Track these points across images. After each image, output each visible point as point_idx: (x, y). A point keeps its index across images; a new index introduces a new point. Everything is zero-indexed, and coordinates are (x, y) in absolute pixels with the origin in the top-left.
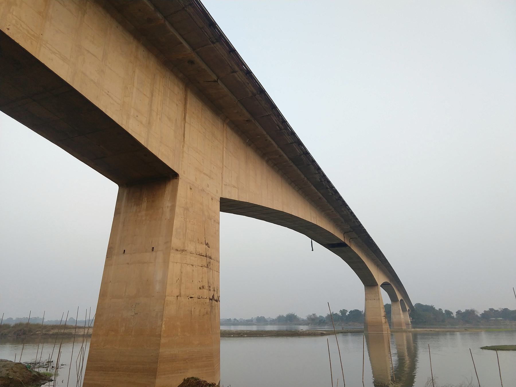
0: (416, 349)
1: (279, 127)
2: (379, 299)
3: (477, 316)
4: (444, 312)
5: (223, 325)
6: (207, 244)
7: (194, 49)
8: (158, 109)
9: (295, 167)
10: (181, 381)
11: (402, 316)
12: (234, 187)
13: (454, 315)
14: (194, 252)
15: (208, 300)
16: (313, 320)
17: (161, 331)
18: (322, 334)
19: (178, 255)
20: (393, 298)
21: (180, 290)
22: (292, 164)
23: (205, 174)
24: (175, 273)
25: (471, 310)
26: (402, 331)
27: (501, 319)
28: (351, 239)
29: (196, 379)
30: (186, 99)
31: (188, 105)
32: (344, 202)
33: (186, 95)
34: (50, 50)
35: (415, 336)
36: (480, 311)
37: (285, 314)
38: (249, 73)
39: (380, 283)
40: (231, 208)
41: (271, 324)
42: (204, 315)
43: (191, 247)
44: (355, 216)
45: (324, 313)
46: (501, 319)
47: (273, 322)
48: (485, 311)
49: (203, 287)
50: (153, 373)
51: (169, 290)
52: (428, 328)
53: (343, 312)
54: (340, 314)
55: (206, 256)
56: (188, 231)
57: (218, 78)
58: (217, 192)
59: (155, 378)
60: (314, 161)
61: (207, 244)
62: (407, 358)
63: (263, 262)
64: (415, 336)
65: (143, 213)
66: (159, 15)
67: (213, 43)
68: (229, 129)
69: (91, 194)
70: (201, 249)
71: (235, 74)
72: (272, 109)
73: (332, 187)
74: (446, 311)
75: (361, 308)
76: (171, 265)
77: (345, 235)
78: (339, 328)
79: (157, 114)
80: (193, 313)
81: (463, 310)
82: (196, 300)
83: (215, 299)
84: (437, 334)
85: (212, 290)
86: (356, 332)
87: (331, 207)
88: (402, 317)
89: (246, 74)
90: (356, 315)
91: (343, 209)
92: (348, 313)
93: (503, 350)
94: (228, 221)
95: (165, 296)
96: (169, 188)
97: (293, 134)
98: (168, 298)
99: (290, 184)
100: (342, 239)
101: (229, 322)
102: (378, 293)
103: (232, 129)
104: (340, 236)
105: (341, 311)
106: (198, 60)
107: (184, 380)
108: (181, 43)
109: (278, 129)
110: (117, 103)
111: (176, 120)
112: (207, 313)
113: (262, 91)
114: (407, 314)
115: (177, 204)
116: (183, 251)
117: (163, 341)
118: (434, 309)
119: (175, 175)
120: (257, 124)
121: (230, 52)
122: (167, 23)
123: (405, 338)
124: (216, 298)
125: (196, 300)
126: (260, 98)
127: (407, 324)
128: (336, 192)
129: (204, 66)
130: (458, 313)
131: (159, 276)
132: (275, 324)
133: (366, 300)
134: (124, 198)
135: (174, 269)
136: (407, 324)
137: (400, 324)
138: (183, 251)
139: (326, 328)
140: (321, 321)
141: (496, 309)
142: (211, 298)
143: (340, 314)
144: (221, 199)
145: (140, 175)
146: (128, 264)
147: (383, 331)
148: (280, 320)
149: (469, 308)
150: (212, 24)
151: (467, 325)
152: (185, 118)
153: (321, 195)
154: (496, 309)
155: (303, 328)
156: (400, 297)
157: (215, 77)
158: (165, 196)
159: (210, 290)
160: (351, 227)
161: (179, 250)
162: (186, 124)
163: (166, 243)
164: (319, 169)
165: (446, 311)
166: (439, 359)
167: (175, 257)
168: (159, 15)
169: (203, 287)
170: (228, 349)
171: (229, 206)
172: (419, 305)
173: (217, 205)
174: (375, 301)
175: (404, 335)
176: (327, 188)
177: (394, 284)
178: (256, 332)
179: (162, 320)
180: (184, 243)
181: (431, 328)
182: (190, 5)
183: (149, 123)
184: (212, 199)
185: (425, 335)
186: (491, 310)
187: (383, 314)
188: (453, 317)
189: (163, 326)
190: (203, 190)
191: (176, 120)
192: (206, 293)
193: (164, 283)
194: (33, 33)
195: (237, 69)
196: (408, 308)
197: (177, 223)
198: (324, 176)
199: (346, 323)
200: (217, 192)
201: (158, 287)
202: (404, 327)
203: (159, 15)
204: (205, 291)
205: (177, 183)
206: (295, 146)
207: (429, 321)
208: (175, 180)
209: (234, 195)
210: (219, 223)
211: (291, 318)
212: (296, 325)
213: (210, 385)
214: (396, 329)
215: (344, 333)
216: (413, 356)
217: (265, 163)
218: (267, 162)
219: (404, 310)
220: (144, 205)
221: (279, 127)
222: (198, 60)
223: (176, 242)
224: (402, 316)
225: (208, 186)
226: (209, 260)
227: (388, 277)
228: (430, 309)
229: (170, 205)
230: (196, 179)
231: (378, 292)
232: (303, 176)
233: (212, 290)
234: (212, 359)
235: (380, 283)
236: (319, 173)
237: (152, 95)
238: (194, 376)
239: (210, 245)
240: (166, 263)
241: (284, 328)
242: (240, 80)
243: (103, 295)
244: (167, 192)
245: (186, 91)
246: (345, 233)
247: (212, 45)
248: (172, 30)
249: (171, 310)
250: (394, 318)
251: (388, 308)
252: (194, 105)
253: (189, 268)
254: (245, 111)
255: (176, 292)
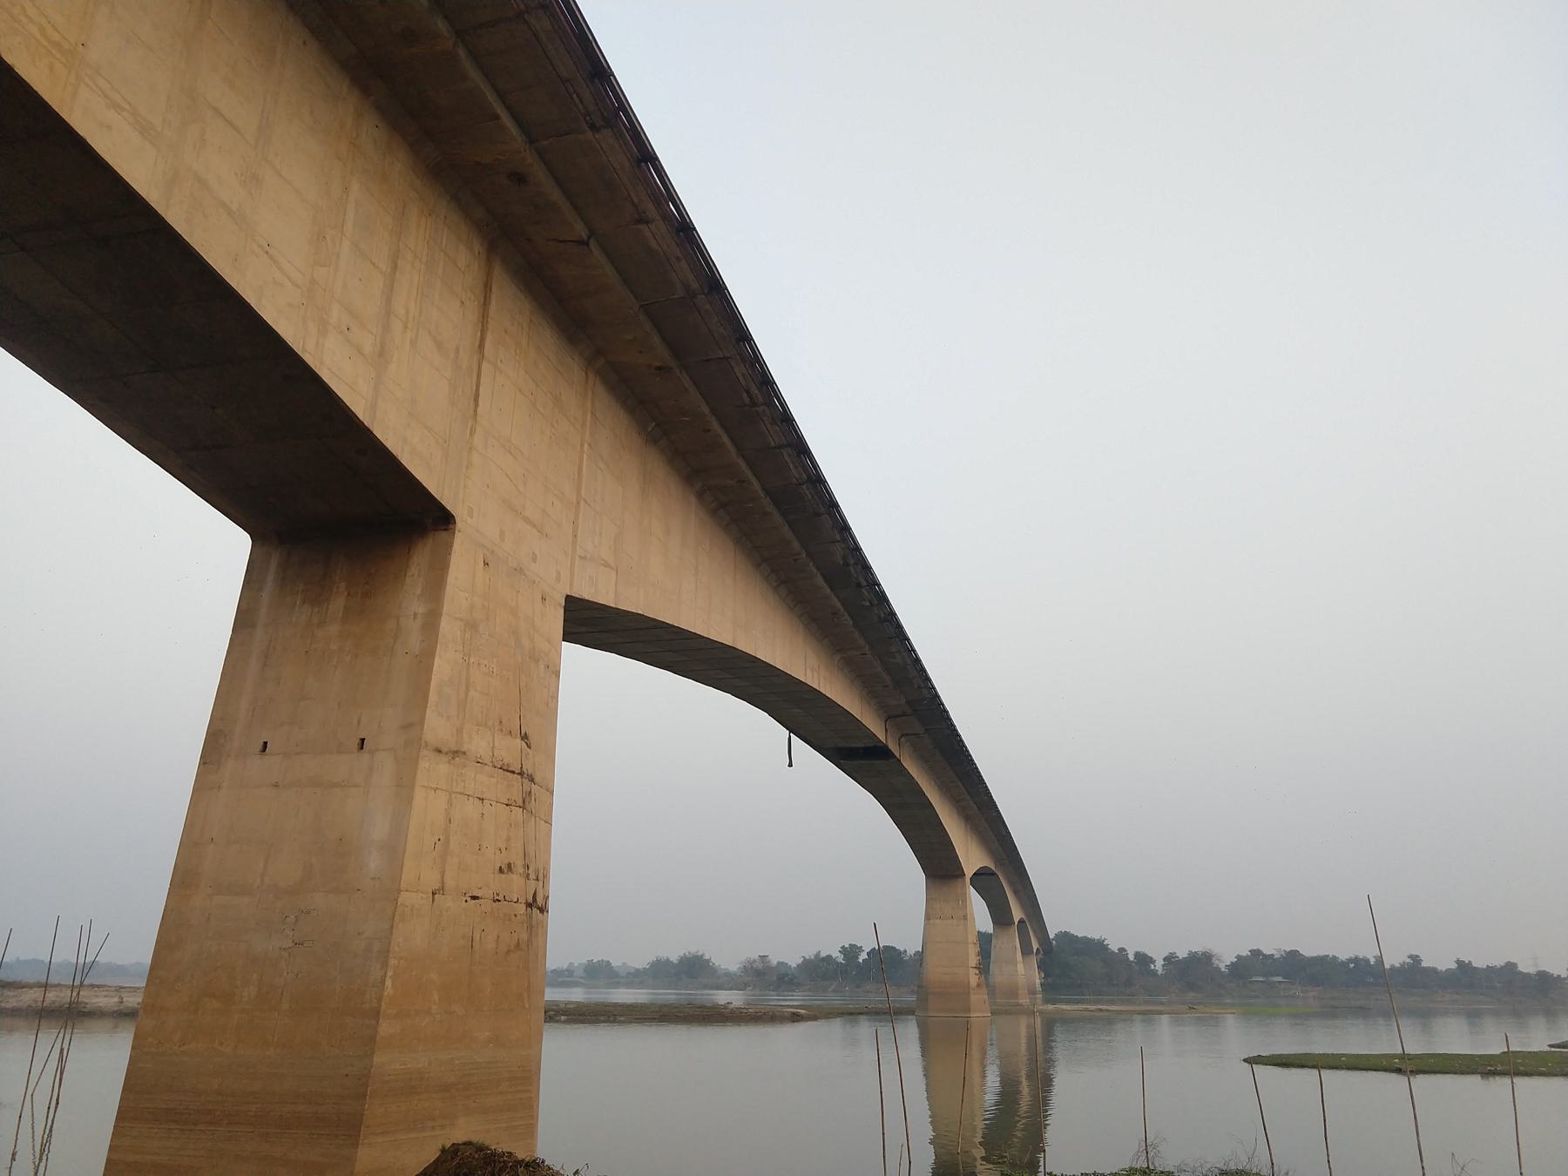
0: (1050, 1063)
1: (750, 397)
2: (965, 918)
3: (1218, 969)
4: (1131, 957)
5: (554, 985)
6: (525, 737)
7: (531, 141)
8: (407, 312)
9: (777, 518)
10: (430, 1155)
11: (1020, 967)
12: (606, 565)
13: (1159, 966)
14: (487, 761)
15: (521, 908)
16: (761, 974)
17: (380, 1000)
18: (796, 1018)
19: (443, 767)
20: (1000, 916)
21: (443, 873)
22: (771, 508)
23: (527, 520)
24: (431, 821)
25: (1204, 954)
26: (1013, 1011)
27: (1280, 979)
28: (903, 736)
29: (481, 1148)
30: (487, 287)
31: (493, 308)
32: (899, 627)
33: (489, 274)
34: (106, 96)
35: (1050, 1024)
36: (1226, 955)
37: (674, 953)
38: (685, 230)
39: (969, 871)
40: (583, 629)
41: (629, 985)
42: (508, 952)
43: (479, 744)
44: (923, 670)
45: (791, 955)
46: (1280, 979)
47: (635, 978)
48: (1238, 957)
49: (509, 865)
50: (349, 1128)
51: (408, 875)
52: (1089, 1003)
53: (851, 952)
54: (841, 959)
55: (521, 774)
56: (472, 693)
57: (592, 233)
58: (558, 579)
59: (356, 1145)
60: (833, 505)
61: (525, 737)
62: (1025, 1089)
63: (671, 799)
64: (1050, 1024)
65: (333, 629)
66: (441, 26)
67: (593, 127)
68: (601, 390)
69: (165, 560)
70: (509, 749)
71: (643, 227)
72: (738, 340)
73: (873, 583)
74: (1137, 954)
75: (909, 940)
76: (419, 794)
77: (884, 721)
78: (835, 1000)
79: (406, 327)
80: (477, 945)
81: (1182, 954)
82: (486, 905)
83: (537, 905)
84: (1109, 1021)
85: (532, 876)
86: (890, 1014)
87: (862, 642)
88: (1024, 972)
89: (678, 231)
90: (886, 962)
91: (893, 649)
92: (863, 956)
93: (1303, 1066)
94: (588, 672)
95: (399, 891)
96: (421, 557)
97: (787, 419)
98: (404, 897)
99: (757, 566)
100: (881, 736)
101: (564, 978)
102: (964, 901)
103: (612, 388)
104: (874, 725)
105: (844, 950)
106: (539, 174)
107: (443, 1151)
108: (497, 117)
109: (747, 401)
110: (295, 285)
111: (457, 351)
112: (518, 946)
113: (715, 286)
114: (1034, 961)
115: (446, 608)
116: (456, 753)
117: (385, 1028)
118: (1106, 948)
119: (442, 519)
120: (687, 383)
121: (639, 161)
122: (462, 53)
123: (1023, 1031)
124: (540, 901)
125: (486, 905)
126: (708, 306)
127: (1032, 992)
128: (882, 598)
129: (556, 195)
130: (1170, 959)
131: (380, 828)
132: (641, 985)
133: (928, 917)
134: (271, 577)
135: (428, 806)
136: (1032, 992)
137: (1013, 992)
138: (456, 753)
139: (794, 1000)
140: (782, 978)
141: (1267, 952)
142: (530, 900)
143: (841, 959)
144: (569, 598)
145: (324, 507)
146: (276, 785)
147: (969, 1010)
148: (661, 971)
149: (1197, 948)
150: (600, 73)
151: (1191, 995)
152: (481, 346)
153: (839, 605)
154: (1267, 950)
155: (723, 997)
156: (1017, 914)
157: (581, 230)
158: (408, 581)
159: (528, 876)
160: (908, 703)
161: (445, 749)
162: (485, 365)
163: (407, 727)
164: (845, 528)
165: (1137, 954)
166: (1099, 1095)
167: (431, 770)
168: (440, 25)
169: (509, 865)
170: (565, 1056)
171: (592, 624)
172: (1065, 937)
173: (555, 620)
174: (955, 922)
175: (1023, 1022)
176: (859, 585)
177: (1006, 877)
178: (685, 999)
179: (385, 965)
180: (460, 731)
181: (1097, 1002)
182: (542, 6)
183: (381, 354)
184: (543, 599)
185: (1067, 1021)
186: (1256, 953)
187: (973, 960)
188: (1154, 973)
189: (389, 983)
190: (519, 570)
191: (457, 351)
192: (516, 886)
193: (394, 850)
194: (56, 37)
195: (651, 210)
196: (1035, 946)
197: (443, 666)
198: (857, 549)
199: (860, 986)
200: (558, 579)
201: (374, 863)
202: (1024, 1001)
203: (440, 25)
204: (516, 879)
205: (449, 546)
206: (787, 454)
207: (1091, 980)
208: (444, 534)
209: (604, 592)
210: (558, 676)
211: (694, 968)
212: (706, 987)
213: (528, 1165)
214: (1005, 1006)
215: (850, 1014)
216: (1043, 1084)
217: (693, 499)
218: (700, 495)
219: (1026, 950)
220: (338, 604)
221: (750, 397)
222: (539, 174)
223: (436, 727)
224: (1020, 967)
225: (534, 560)
226: (528, 785)
227: (992, 853)
228: (1096, 948)
229: (420, 609)
230: (502, 533)
231: (964, 898)
232: (796, 545)
233: (532, 876)
234: (523, 1083)
235: (969, 871)
236: (844, 540)
237: (395, 267)
238: (475, 1138)
239: (532, 741)
240: (404, 787)
241: (669, 995)
242: (653, 243)
243: (184, 879)
244: (413, 570)
245: (489, 261)
246: (889, 718)
247: (590, 134)
248: (474, 74)
249: (412, 935)
250: (999, 974)
251: (985, 940)
252: (509, 305)
253: (471, 808)
254: (656, 339)
255: (431, 879)
